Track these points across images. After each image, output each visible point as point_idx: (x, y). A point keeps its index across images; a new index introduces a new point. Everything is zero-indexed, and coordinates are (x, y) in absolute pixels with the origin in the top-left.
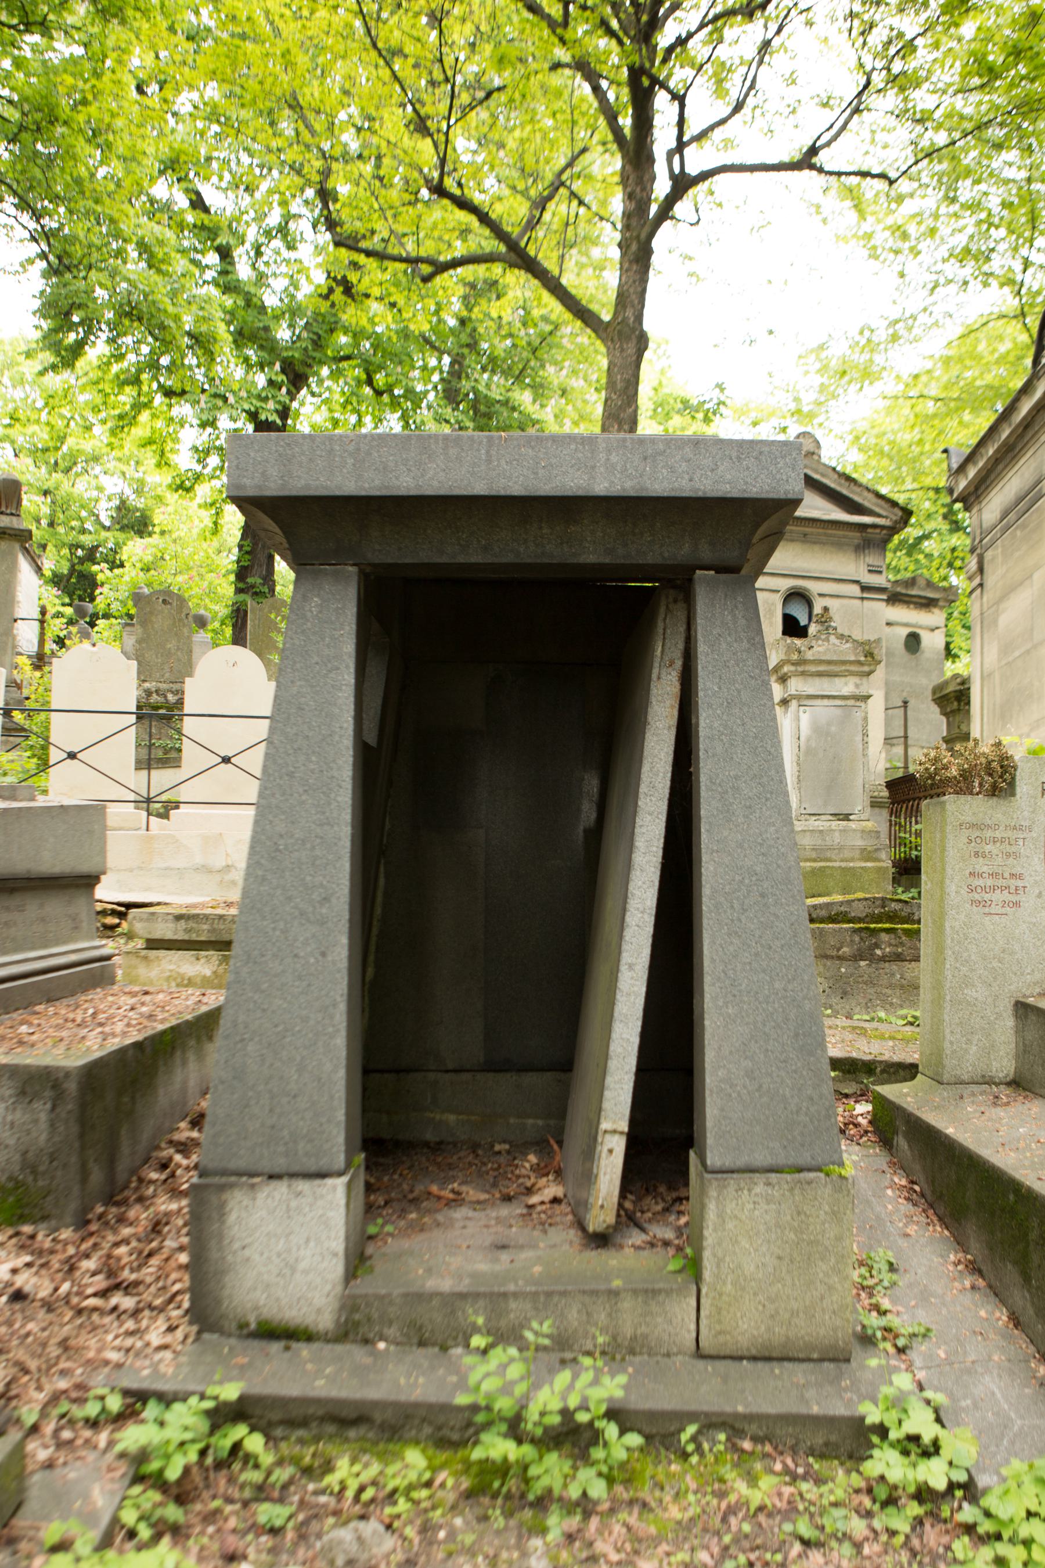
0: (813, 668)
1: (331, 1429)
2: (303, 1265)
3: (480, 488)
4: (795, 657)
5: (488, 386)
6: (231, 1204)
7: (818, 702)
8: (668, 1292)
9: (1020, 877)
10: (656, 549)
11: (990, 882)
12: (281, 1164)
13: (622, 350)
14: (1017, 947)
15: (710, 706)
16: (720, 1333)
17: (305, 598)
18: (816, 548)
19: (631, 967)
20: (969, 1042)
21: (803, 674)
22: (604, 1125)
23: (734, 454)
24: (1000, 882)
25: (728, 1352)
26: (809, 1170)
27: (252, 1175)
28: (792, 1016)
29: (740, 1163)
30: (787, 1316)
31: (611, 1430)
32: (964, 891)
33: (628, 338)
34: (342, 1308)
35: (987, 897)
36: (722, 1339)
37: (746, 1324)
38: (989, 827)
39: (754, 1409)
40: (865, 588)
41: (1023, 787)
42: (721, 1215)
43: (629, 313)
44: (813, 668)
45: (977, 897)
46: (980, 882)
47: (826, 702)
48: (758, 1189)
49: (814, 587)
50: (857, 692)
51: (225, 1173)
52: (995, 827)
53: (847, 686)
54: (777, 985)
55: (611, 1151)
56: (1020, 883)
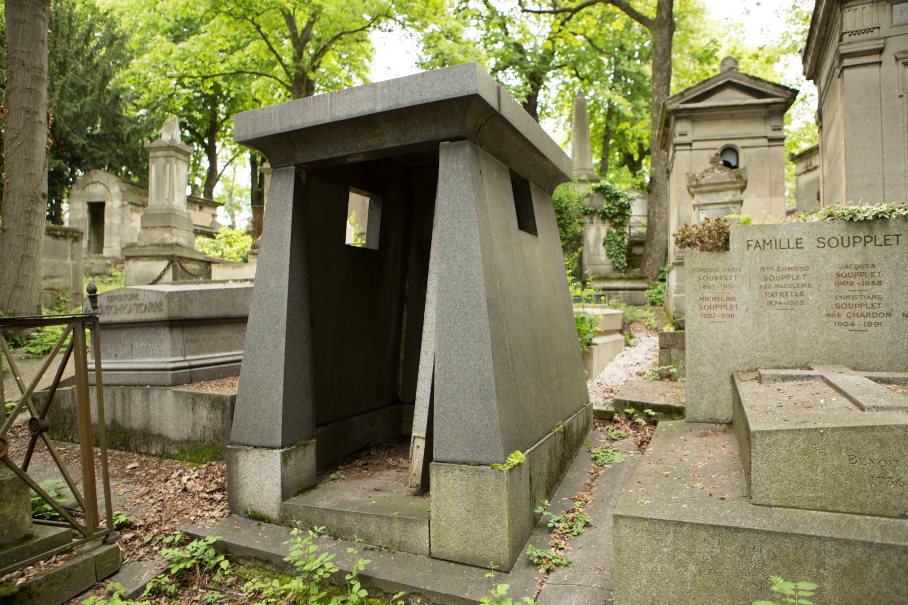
0: (706, 189)
1: (260, 564)
2: (266, 488)
3: (328, 119)
4: (694, 183)
5: (629, 66)
6: (240, 458)
7: (711, 207)
8: (415, 522)
9: (734, 299)
10: (418, 135)
11: (713, 303)
12: (258, 442)
13: (661, 33)
14: (732, 342)
15: (443, 214)
16: (440, 546)
17: (275, 184)
18: (739, 121)
19: (426, 353)
20: (702, 398)
21: (701, 192)
22: (414, 434)
23: (441, 77)
24: (720, 303)
25: (444, 557)
26: (485, 465)
27: (248, 446)
28: (478, 380)
29: (449, 458)
30: (473, 543)
31: (357, 586)
32: (697, 309)
33: (664, 26)
34: (281, 510)
35: (711, 312)
36: (441, 550)
37: (453, 545)
38: (712, 270)
39: (436, 590)
40: (771, 140)
41: (733, 245)
42: (438, 484)
43: (664, 14)
44: (706, 189)
45: (705, 312)
46: (707, 303)
47: (715, 207)
48: (456, 472)
49: (738, 144)
50: (734, 199)
51: (239, 444)
52: (717, 270)
53: (727, 197)
54: (471, 363)
55: (418, 447)
56: (734, 303)
